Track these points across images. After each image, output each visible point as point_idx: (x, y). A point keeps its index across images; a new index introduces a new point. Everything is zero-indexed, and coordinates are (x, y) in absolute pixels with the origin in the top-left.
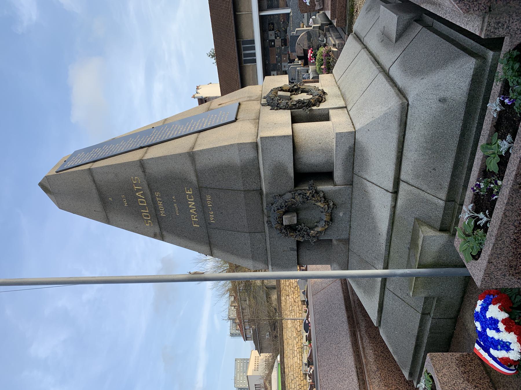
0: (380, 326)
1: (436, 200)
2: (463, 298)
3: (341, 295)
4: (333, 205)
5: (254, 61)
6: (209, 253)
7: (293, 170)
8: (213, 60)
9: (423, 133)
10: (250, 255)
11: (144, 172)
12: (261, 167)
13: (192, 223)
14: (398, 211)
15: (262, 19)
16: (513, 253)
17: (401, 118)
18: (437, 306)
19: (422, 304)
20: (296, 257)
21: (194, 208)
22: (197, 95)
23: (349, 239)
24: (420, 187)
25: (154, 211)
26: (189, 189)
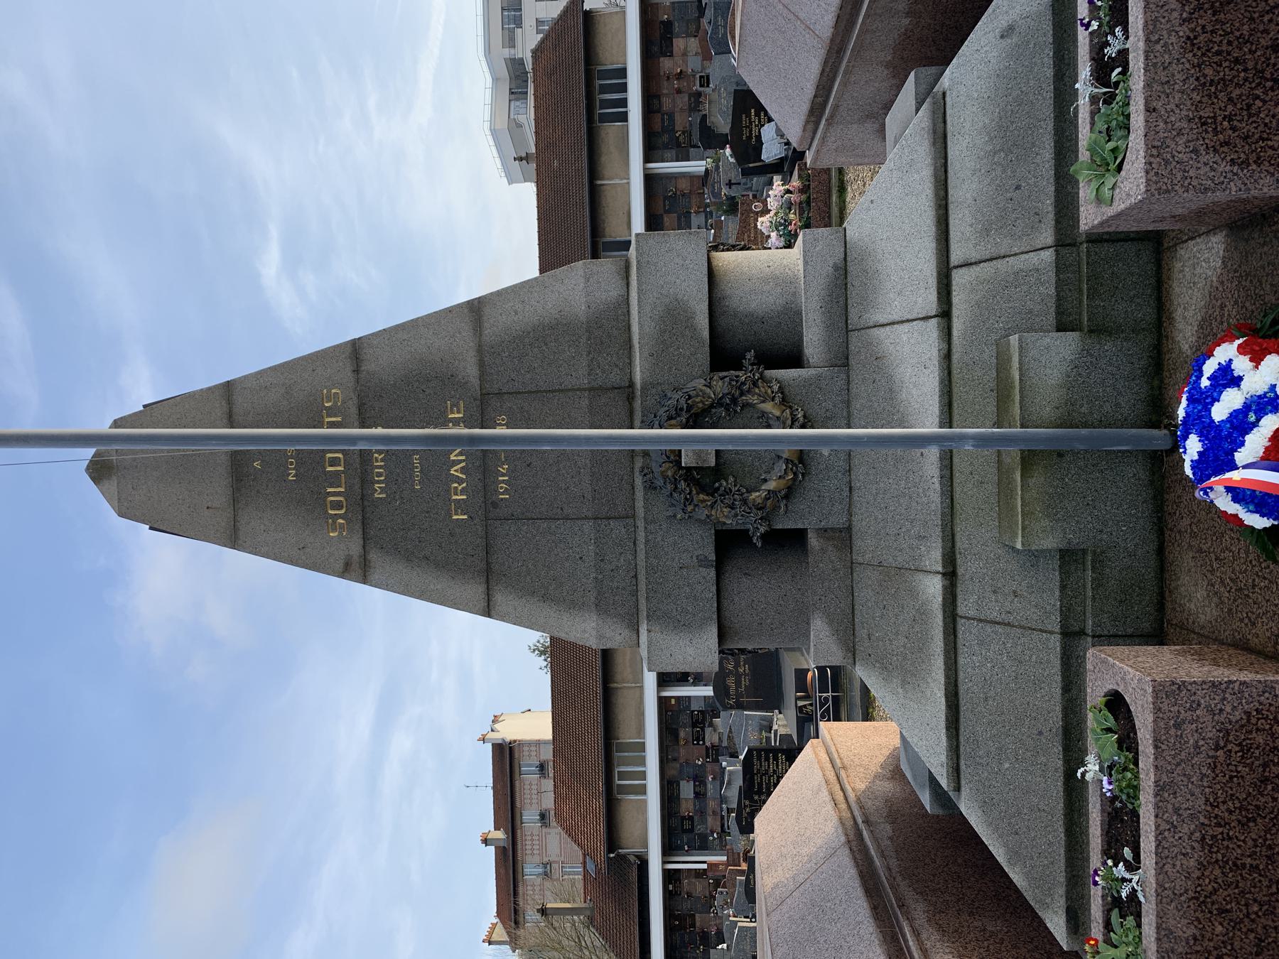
0: (958, 789)
1: (1034, 258)
2: (1160, 550)
3: (850, 874)
4: (805, 416)
5: (624, 117)
6: (483, 604)
7: (707, 321)
8: (541, 661)
9: (981, 124)
10: (592, 597)
11: (357, 371)
12: (635, 328)
13: (450, 509)
14: (955, 357)
15: (663, 703)
16: (1197, 79)
17: (934, 125)
18: (1098, 584)
19: (1057, 593)
20: (714, 589)
21: (461, 461)
22: (491, 735)
23: (849, 529)
24: (994, 252)
25: (357, 487)
26: (457, 405)
